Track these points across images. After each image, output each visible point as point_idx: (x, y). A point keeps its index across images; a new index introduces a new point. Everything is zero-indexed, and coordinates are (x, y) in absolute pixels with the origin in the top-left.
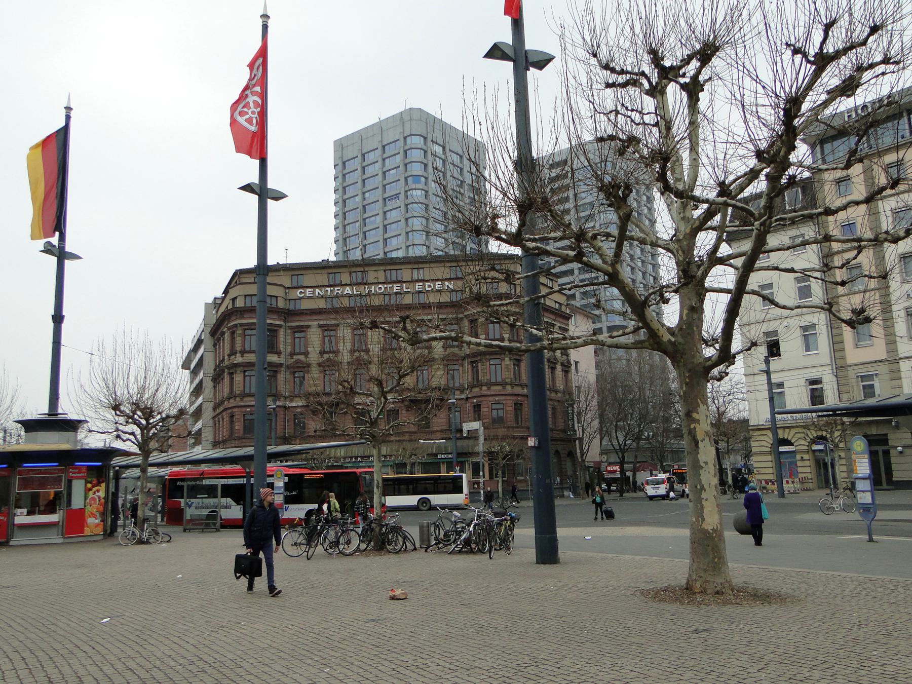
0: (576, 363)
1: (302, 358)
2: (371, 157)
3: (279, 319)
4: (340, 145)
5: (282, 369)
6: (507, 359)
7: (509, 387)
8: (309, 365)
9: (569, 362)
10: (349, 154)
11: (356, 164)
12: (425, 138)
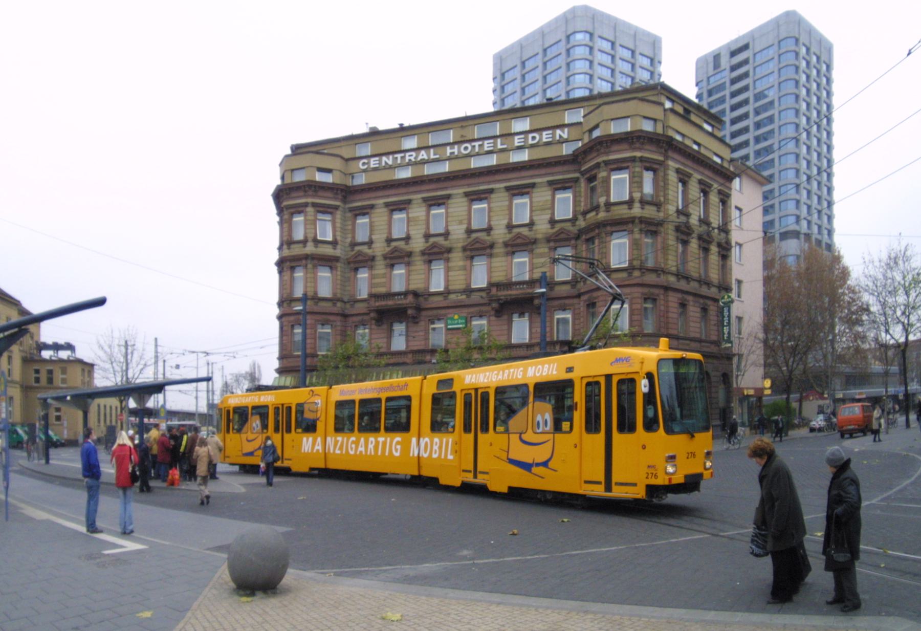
0: (739, 282)
1: (364, 249)
2: (530, 65)
3: (336, 199)
4: (500, 59)
5: (339, 265)
6: (636, 230)
7: (636, 273)
8: (373, 258)
9: (728, 243)
10: (508, 65)
11: (517, 73)
12: (591, 35)
